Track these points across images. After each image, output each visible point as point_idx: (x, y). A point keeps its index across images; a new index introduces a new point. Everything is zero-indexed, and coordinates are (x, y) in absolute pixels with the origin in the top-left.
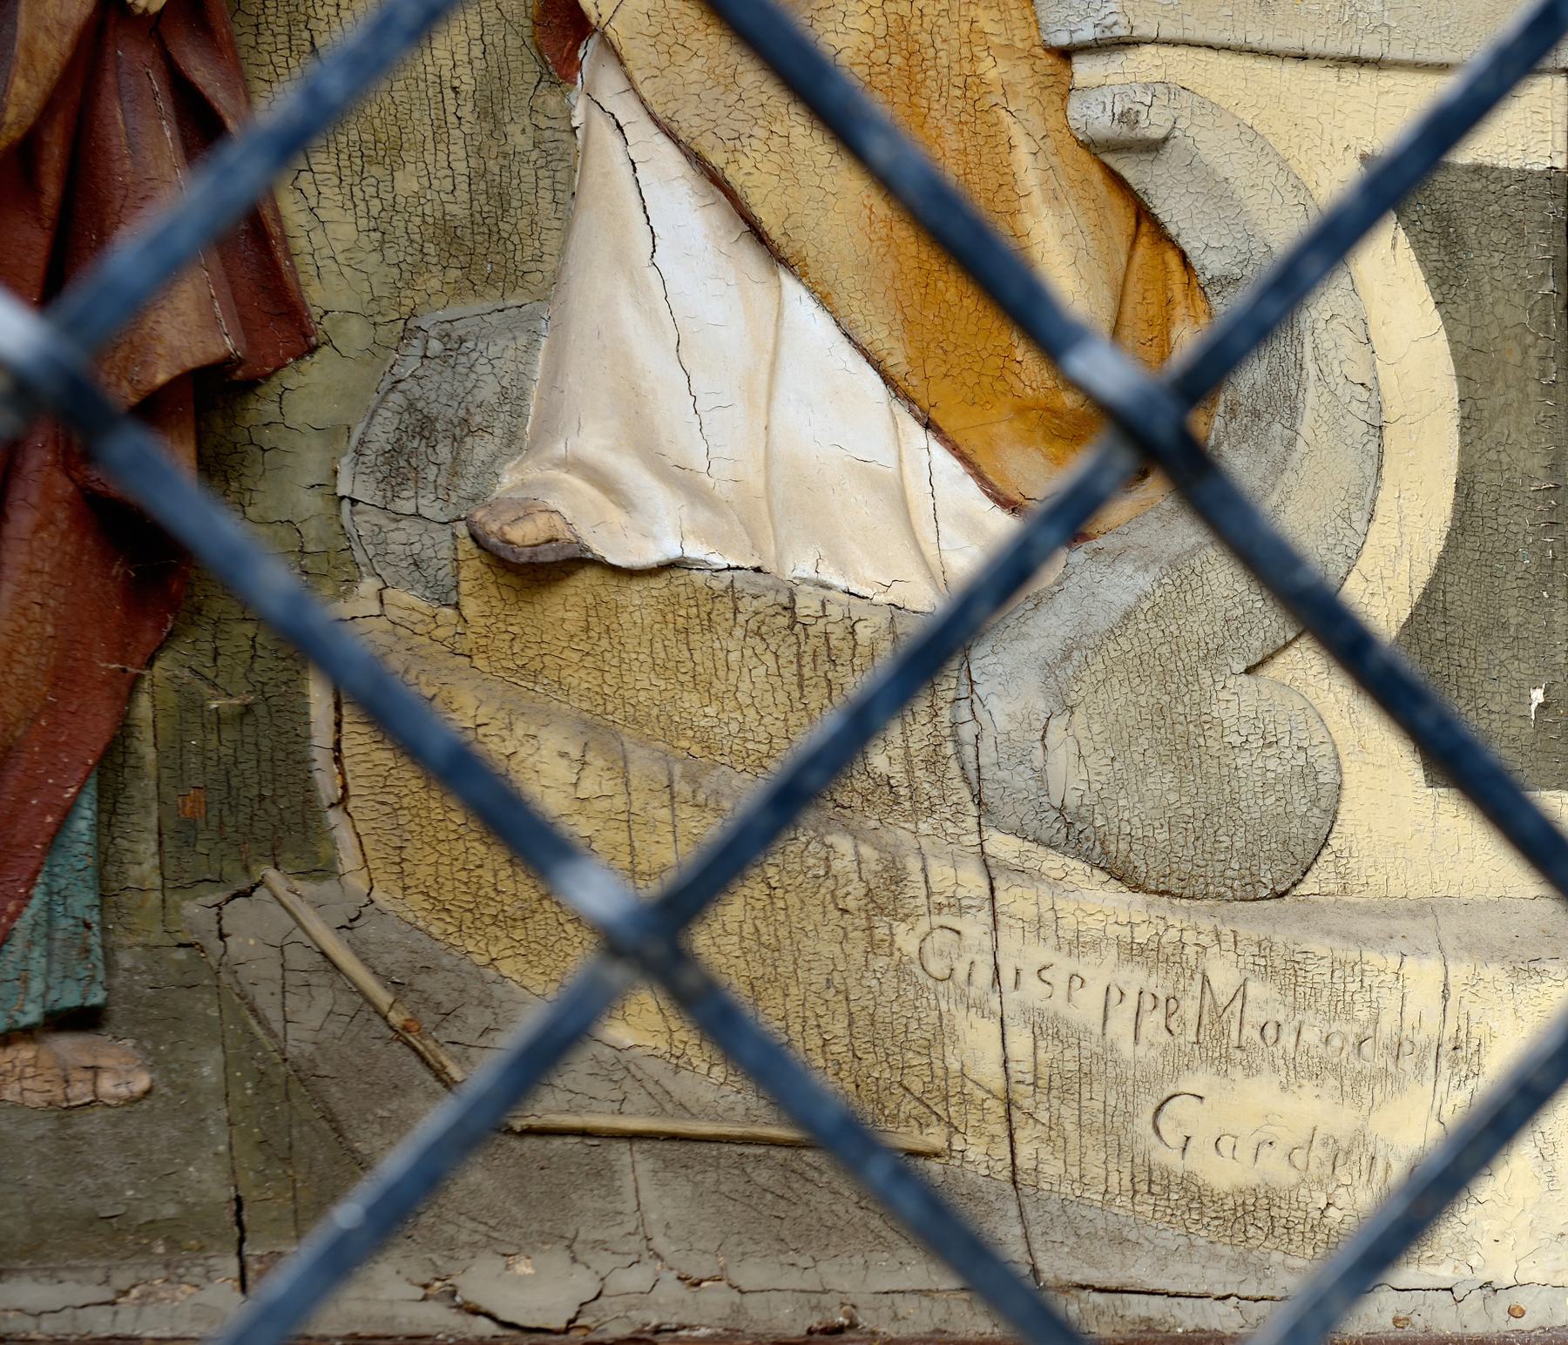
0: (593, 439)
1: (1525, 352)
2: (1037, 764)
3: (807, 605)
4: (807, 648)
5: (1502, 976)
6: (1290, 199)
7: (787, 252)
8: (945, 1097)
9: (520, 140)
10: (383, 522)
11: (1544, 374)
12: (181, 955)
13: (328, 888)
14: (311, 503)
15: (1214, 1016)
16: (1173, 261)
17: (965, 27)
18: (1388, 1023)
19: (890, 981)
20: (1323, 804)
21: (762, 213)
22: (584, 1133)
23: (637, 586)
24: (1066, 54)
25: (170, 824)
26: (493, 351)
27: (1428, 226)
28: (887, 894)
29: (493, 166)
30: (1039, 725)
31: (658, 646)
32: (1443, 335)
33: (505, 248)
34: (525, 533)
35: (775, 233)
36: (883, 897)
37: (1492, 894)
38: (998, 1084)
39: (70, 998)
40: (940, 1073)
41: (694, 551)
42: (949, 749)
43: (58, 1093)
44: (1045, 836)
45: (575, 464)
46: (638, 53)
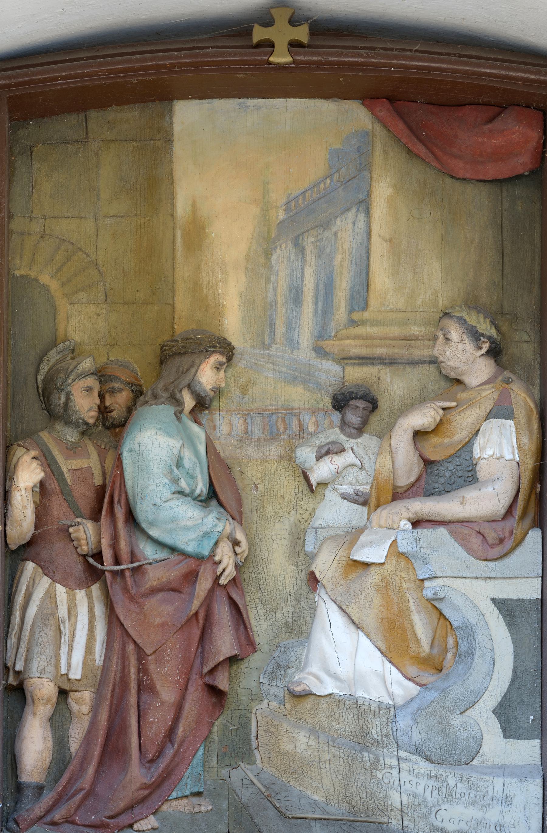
0: (314, 668)
1: (530, 640)
2: (410, 735)
3: (360, 702)
4: (360, 712)
5: (518, 781)
6: (473, 609)
7: (359, 626)
8: (388, 810)
9: (303, 604)
10: (269, 687)
11: (535, 645)
12: (221, 781)
13: (254, 767)
14: (254, 684)
15: (449, 791)
16: (448, 624)
17: (399, 576)
18: (490, 792)
19: (376, 784)
20: (478, 743)
21: (353, 618)
22: (305, 818)
23: (323, 699)
24: (423, 580)
25: (220, 754)
26: (295, 650)
27: (507, 613)
28: (375, 765)
29: (298, 611)
30: (410, 727)
31: (327, 712)
32: (510, 637)
33: (299, 628)
34: (298, 689)
35: (357, 622)
36: (374, 766)
37: (520, 763)
38: (399, 807)
39: (196, 790)
40: (386, 805)
41: (336, 691)
42: (391, 733)
43: (192, 810)
44: (412, 752)
45: (310, 674)
46: (329, 586)
